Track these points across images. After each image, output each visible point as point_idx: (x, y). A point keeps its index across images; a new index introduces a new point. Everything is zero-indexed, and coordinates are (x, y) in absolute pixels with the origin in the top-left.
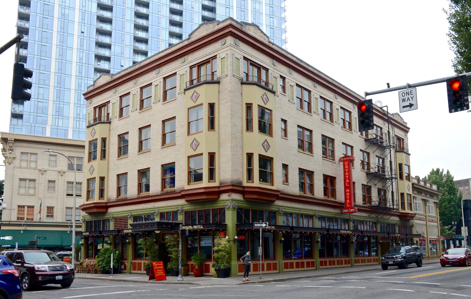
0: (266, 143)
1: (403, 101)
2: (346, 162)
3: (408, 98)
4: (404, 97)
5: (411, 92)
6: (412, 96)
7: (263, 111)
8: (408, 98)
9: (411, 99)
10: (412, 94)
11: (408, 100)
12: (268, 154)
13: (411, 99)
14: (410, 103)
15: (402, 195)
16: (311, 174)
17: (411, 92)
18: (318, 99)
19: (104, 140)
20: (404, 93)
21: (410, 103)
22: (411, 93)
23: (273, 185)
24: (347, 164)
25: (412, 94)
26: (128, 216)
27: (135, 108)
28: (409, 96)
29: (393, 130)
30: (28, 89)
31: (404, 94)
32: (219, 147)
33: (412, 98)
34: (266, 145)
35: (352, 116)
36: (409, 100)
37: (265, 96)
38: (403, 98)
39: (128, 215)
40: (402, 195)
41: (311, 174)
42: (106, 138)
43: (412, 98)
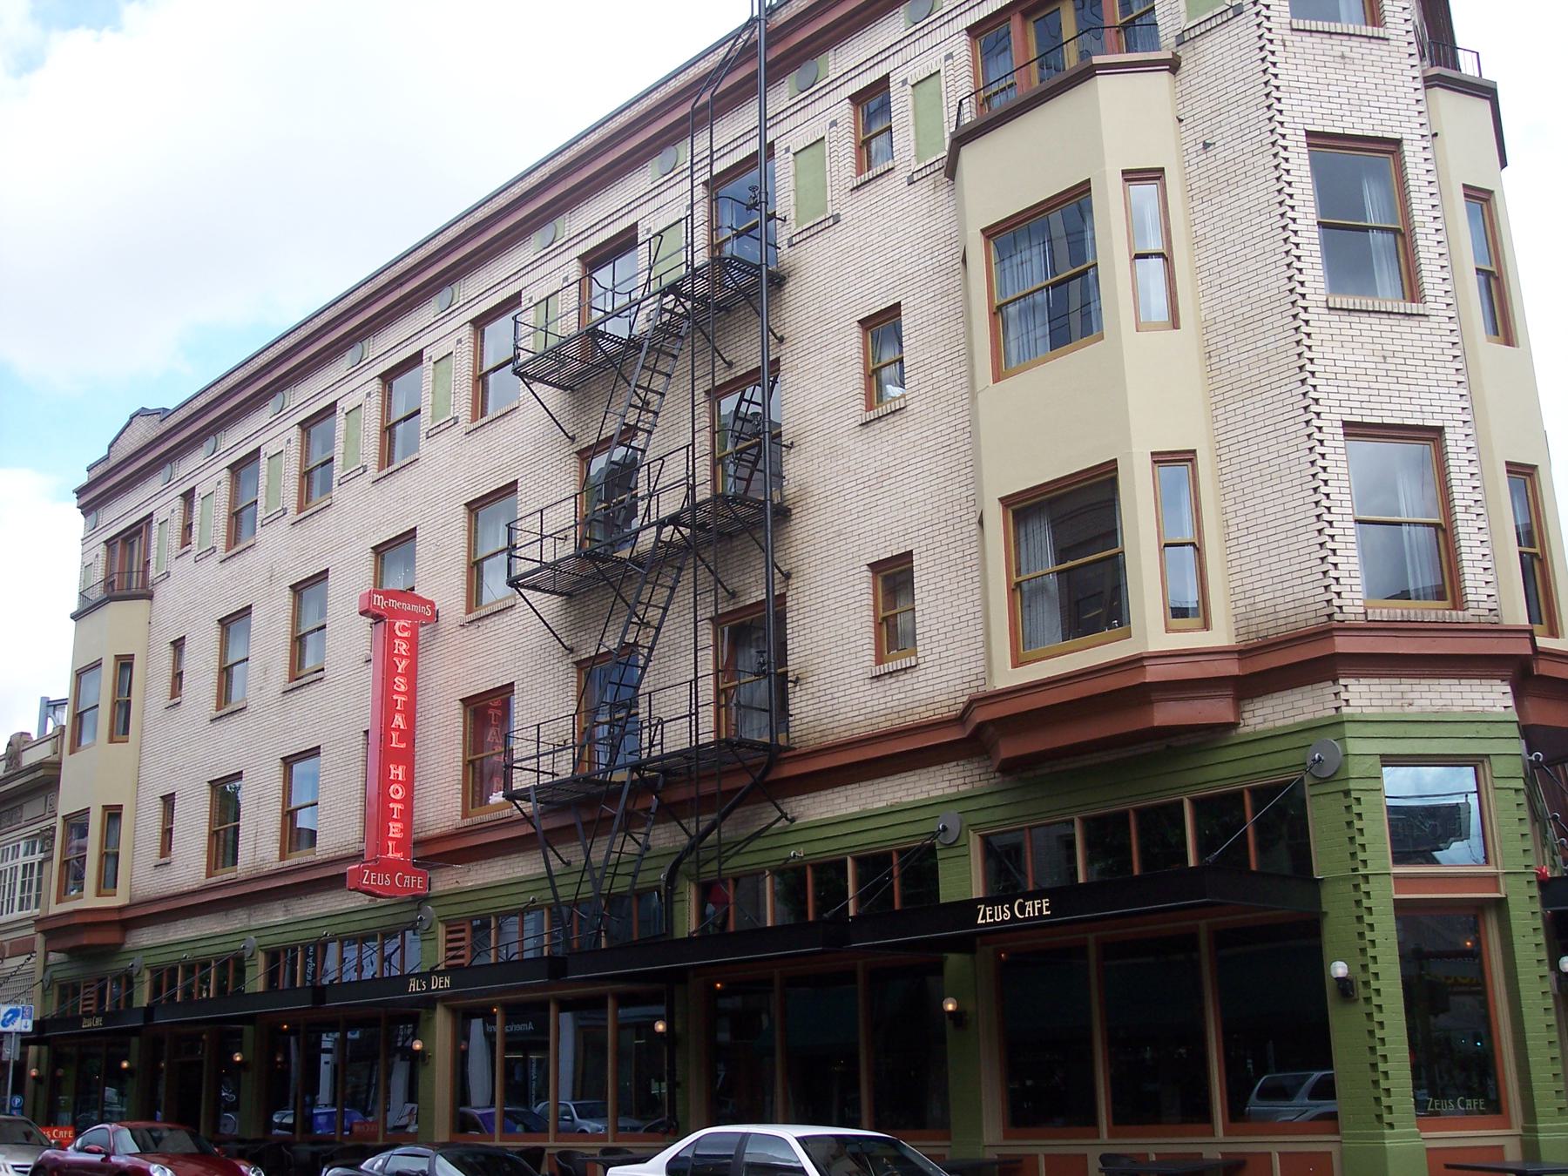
2: (403, 623)
24: (406, 634)
27: (449, 414)
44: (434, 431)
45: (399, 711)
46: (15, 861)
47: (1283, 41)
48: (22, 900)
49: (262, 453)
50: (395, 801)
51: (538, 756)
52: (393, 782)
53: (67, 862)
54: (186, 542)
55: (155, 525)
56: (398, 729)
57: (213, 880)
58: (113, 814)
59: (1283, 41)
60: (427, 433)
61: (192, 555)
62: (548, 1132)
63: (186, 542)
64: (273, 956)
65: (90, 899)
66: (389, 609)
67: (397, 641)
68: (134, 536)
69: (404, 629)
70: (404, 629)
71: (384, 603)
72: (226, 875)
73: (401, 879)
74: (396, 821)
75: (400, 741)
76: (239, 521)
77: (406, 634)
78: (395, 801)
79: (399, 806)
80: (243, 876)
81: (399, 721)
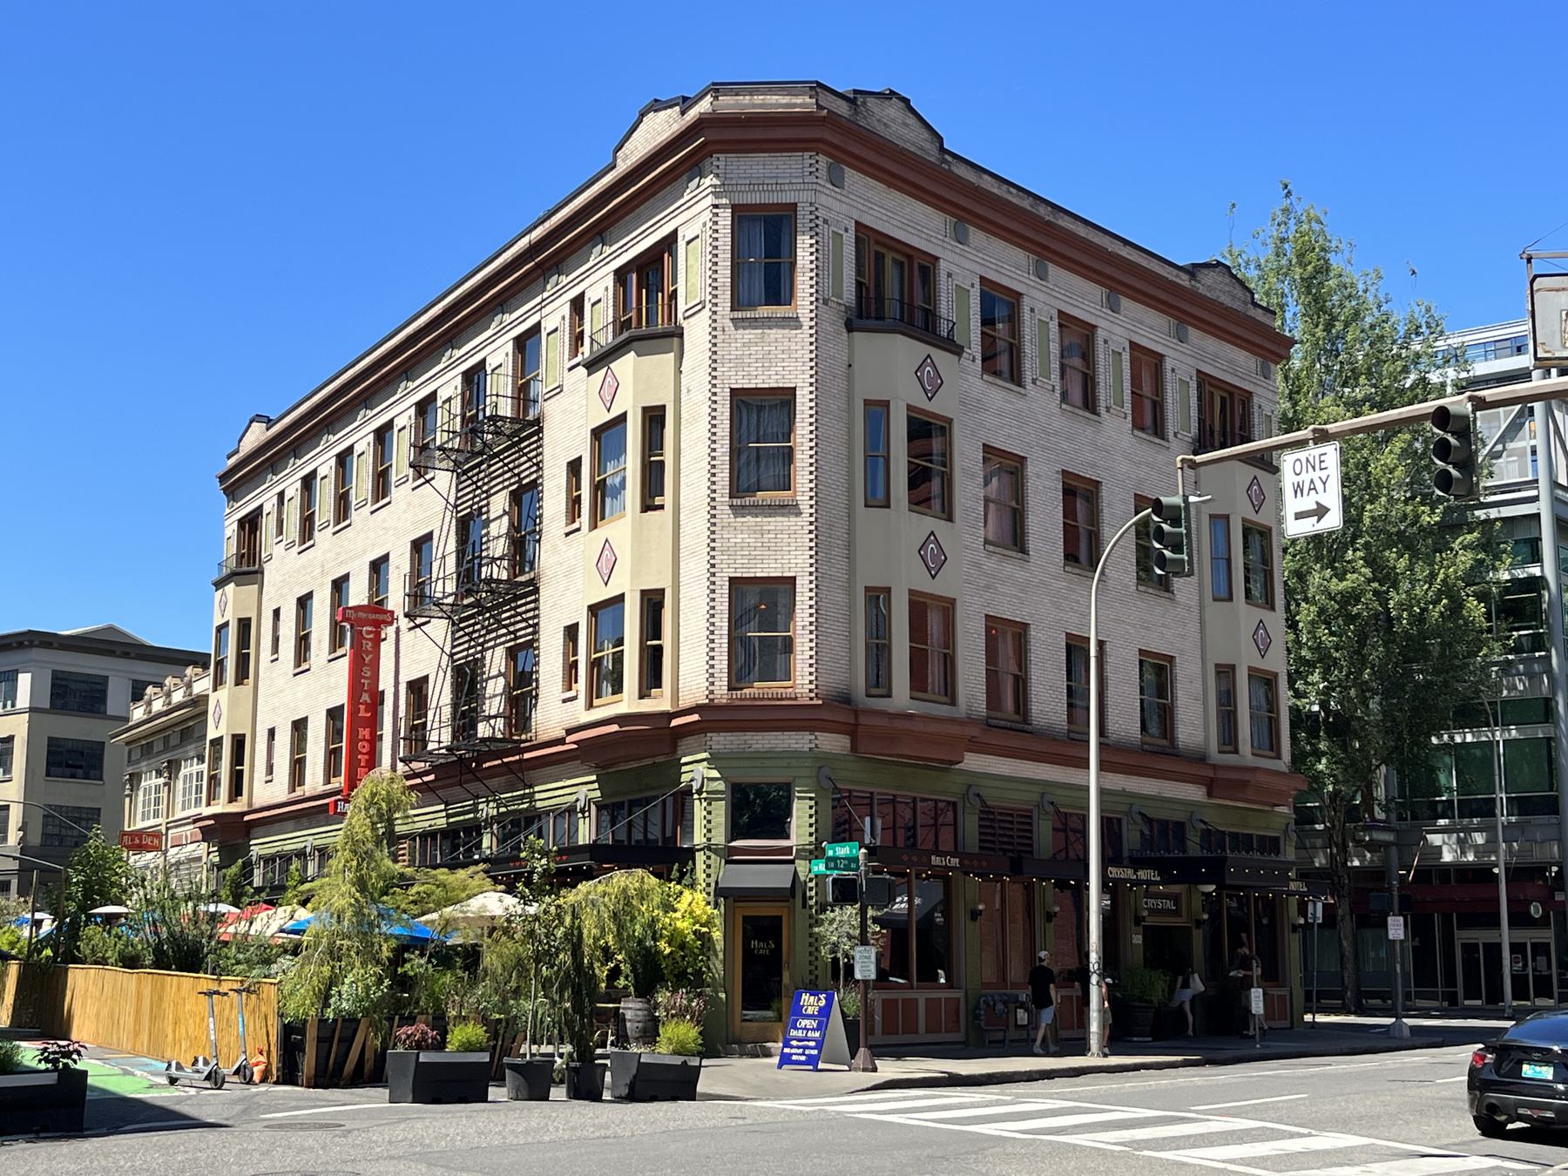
0: (932, 545)
1: (1296, 492)
3: (1312, 481)
4: (1300, 479)
5: (1323, 458)
6: (1323, 474)
7: (919, 606)
8: (1312, 481)
9: (1319, 486)
10: (1323, 465)
11: (1310, 489)
12: (935, 407)
13: (1319, 486)
14: (1317, 503)
15: (1226, 673)
16: (1020, 632)
17: (1323, 458)
18: (1124, 353)
19: (653, 603)
20: (1298, 463)
21: (1317, 503)
22: (1321, 462)
23: (953, 702)
24: (371, 636)
25: (1323, 465)
26: (694, 783)
28: (1315, 475)
29: (1430, 856)
30: (381, 689)
31: (1298, 463)
32: (851, 531)
33: (1324, 483)
34: (935, 561)
35: (1169, 374)
36: (1315, 489)
37: (928, 368)
38: (1296, 479)
39: (692, 780)
40: (1226, 673)
41: (1020, 632)
42: (661, 592)
43: (1324, 483)
45: (365, 691)
46: (148, 782)
47: (723, 328)
48: (184, 802)
49: (680, 238)
50: (361, 753)
51: (440, 728)
53: (598, 661)
54: (280, 532)
55: (681, 244)
56: (365, 703)
57: (329, 786)
59: (723, 328)
60: (704, 307)
61: (284, 543)
62: (1511, 944)
63: (280, 532)
64: (1222, 706)
65: (628, 702)
67: (364, 642)
68: (250, 524)
69: (369, 632)
71: (354, 615)
72: (299, 792)
74: (363, 767)
75: (366, 711)
76: (382, 485)
77: (371, 636)
78: (361, 753)
79: (367, 757)
80: (308, 794)
81: (366, 697)
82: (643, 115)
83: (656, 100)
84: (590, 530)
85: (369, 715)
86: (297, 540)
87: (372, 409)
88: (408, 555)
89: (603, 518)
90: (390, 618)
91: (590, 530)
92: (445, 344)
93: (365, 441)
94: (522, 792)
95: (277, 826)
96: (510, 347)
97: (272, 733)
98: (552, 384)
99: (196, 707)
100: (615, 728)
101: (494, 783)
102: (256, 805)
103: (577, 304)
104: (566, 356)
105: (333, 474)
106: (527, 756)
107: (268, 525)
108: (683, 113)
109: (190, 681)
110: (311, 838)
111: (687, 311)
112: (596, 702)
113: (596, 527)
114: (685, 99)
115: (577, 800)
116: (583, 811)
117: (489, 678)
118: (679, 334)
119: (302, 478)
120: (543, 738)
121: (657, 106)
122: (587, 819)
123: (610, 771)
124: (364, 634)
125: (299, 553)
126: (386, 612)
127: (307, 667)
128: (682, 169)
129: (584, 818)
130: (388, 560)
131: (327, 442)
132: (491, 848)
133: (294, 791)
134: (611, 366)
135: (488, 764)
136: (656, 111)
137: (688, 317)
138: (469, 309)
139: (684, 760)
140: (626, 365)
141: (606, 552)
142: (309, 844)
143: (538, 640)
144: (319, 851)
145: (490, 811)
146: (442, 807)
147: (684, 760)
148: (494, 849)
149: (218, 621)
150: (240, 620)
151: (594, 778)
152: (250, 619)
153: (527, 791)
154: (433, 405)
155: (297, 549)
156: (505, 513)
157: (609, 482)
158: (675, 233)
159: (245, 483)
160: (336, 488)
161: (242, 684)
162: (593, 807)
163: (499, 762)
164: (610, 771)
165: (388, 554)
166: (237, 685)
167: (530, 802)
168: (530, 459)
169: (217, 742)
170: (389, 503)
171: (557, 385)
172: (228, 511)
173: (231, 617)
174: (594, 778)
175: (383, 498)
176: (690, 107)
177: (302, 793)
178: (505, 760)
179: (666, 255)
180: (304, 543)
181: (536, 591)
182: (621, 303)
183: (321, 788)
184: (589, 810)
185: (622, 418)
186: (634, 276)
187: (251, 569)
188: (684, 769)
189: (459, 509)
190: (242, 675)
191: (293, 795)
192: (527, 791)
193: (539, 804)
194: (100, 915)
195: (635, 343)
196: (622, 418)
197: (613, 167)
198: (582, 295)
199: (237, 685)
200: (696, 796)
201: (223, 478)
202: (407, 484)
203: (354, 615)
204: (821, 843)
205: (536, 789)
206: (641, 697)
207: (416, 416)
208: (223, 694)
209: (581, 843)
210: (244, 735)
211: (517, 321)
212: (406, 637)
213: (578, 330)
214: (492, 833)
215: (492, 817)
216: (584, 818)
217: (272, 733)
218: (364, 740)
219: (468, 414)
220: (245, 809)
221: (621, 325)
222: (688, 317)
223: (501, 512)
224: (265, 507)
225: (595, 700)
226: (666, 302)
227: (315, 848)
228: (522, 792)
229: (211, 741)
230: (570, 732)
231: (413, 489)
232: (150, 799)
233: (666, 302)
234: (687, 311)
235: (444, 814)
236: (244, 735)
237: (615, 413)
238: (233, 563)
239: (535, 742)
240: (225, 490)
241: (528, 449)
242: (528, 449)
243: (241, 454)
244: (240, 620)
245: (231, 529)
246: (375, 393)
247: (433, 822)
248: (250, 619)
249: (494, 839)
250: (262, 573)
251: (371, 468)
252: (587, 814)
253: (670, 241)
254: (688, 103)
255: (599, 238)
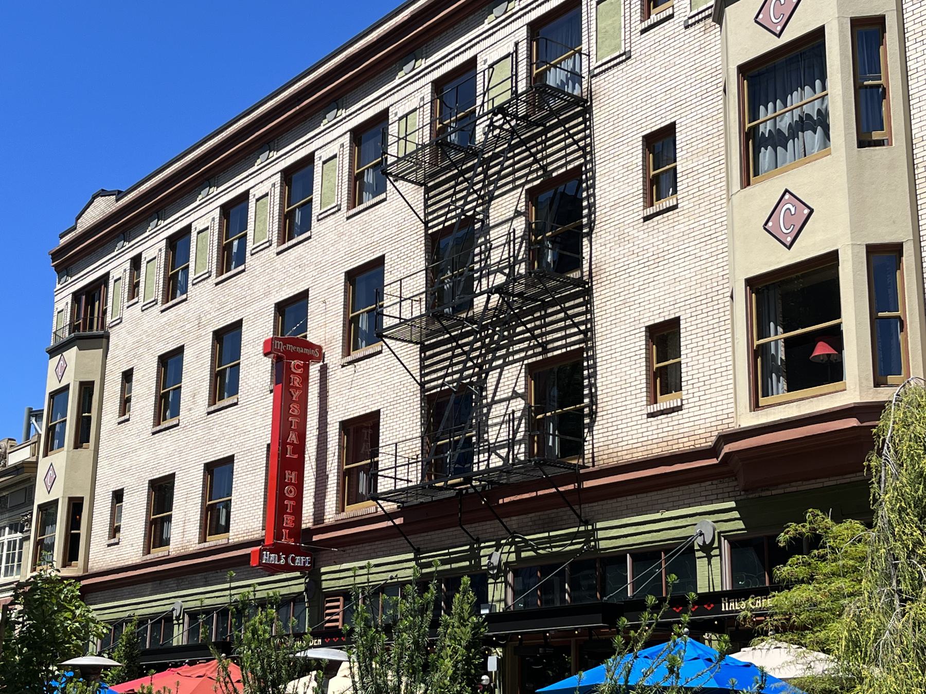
24: (299, 371)
44: (693, 20)
49: (251, 197)
52: (287, 484)
55: (111, 282)
56: (292, 444)
58: (76, 506)
66: (286, 352)
70: (298, 367)
71: (283, 347)
73: (293, 560)
75: (294, 453)
77: (299, 371)
79: (292, 503)
80: (173, 554)
82: (94, 198)
83: (103, 190)
84: (743, 187)
85: (295, 456)
86: (160, 298)
87: (129, 242)
88: (341, 287)
89: (756, 174)
90: (315, 353)
91: (743, 187)
92: (118, 236)
93: (65, 301)
94: (575, 530)
95: (126, 590)
96: (216, 214)
97: (118, 496)
98: (149, 298)
99: (18, 475)
100: (853, 422)
101: (513, 522)
102: (90, 571)
103: (136, 262)
104: (126, 300)
105: (216, 227)
106: (587, 484)
107: (116, 293)
108: (117, 200)
109: (5, 452)
110: (180, 600)
111: (253, 249)
112: (763, 401)
113: (749, 184)
114: (119, 192)
115: (174, 609)
116: (178, 618)
117: (494, 402)
118: (107, 337)
119: (167, 238)
120: (601, 463)
121: (103, 193)
122: (181, 626)
123: (763, 494)
124: (292, 366)
125: (162, 311)
126: (311, 346)
127: (175, 422)
128: (318, 106)
129: (179, 624)
130: (307, 296)
131: (65, 282)
132: (505, 600)
133: (149, 553)
134: (64, 354)
135: (507, 500)
136: (102, 196)
137: (322, 219)
138: (425, 25)
139: (323, 570)
140: (72, 354)
141: (51, 472)
142: (178, 607)
143: (593, 348)
144: (188, 613)
145: (504, 557)
146: (411, 556)
147: (323, 570)
148: (510, 603)
149: (53, 385)
150: (82, 384)
151: (732, 504)
152: (93, 382)
153: (582, 528)
154: (473, 71)
155: (159, 307)
156: (518, 214)
157: (762, 129)
158: (108, 274)
159: (85, 256)
160: (220, 238)
161: (81, 447)
162: (725, 545)
163: (554, 490)
164: (763, 494)
165: (307, 291)
166: (76, 447)
167: (585, 543)
168: (576, 142)
169: (49, 509)
170: (310, 238)
171: (153, 299)
172: (58, 286)
173: (71, 379)
174: (732, 504)
175: (288, 241)
176: (122, 197)
177: (166, 553)
178: (561, 489)
179: (103, 287)
180: (222, 274)
181: (589, 292)
182: (75, 314)
183: (194, 545)
184: (183, 619)
185: (67, 388)
186: (84, 297)
187: (88, 333)
188: (324, 577)
189: (430, 225)
190: (82, 438)
191: (149, 557)
192: (582, 528)
193: (603, 544)
194: (74, 667)
195: (78, 341)
196: (67, 388)
197: (74, 228)
198: (140, 255)
199: (76, 447)
200: (175, 622)
201: (55, 255)
202: (271, 248)
203: (283, 347)
204: (628, 633)
205: (599, 525)
206: (877, 384)
207: (72, 302)
208: (59, 459)
209: (175, 644)
210: (82, 498)
211: (173, 225)
212: (337, 376)
213: (135, 281)
214: (506, 582)
215: (507, 564)
216: (179, 624)
217: (118, 496)
218: (291, 484)
219: (535, 72)
220: (81, 574)
221: (73, 327)
222: (322, 219)
223: (511, 214)
224: (143, 256)
225: (760, 399)
226: (100, 315)
227: (185, 611)
228: (575, 530)
229: (40, 506)
230: (726, 438)
231: (348, 218)
232: (14, 554)
233: (100, 315)
234: (253, 249)
235: (413, 564)
236: (82, 498)
237: (63, 384)
238: (66, 335)
239: (591, 469)
240: (56, 267)
241: (575, 130)
242: (575, 130)
243: (79, 230)
244: (82, 384)
245: (63, 301)
246: (281, 134)
247: (394, 574)
248: (93, 382)
249: (510, 590)
250: (108, 338)
251: (277, 208)
252: (181, 621)
253: (105, 278)
254: (121, 195)
255: (122, 236)
